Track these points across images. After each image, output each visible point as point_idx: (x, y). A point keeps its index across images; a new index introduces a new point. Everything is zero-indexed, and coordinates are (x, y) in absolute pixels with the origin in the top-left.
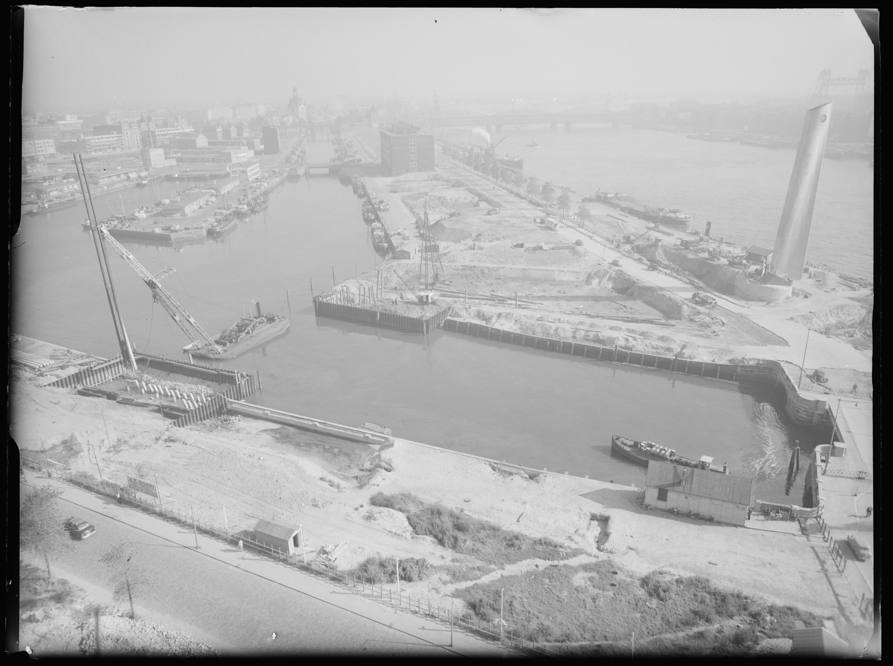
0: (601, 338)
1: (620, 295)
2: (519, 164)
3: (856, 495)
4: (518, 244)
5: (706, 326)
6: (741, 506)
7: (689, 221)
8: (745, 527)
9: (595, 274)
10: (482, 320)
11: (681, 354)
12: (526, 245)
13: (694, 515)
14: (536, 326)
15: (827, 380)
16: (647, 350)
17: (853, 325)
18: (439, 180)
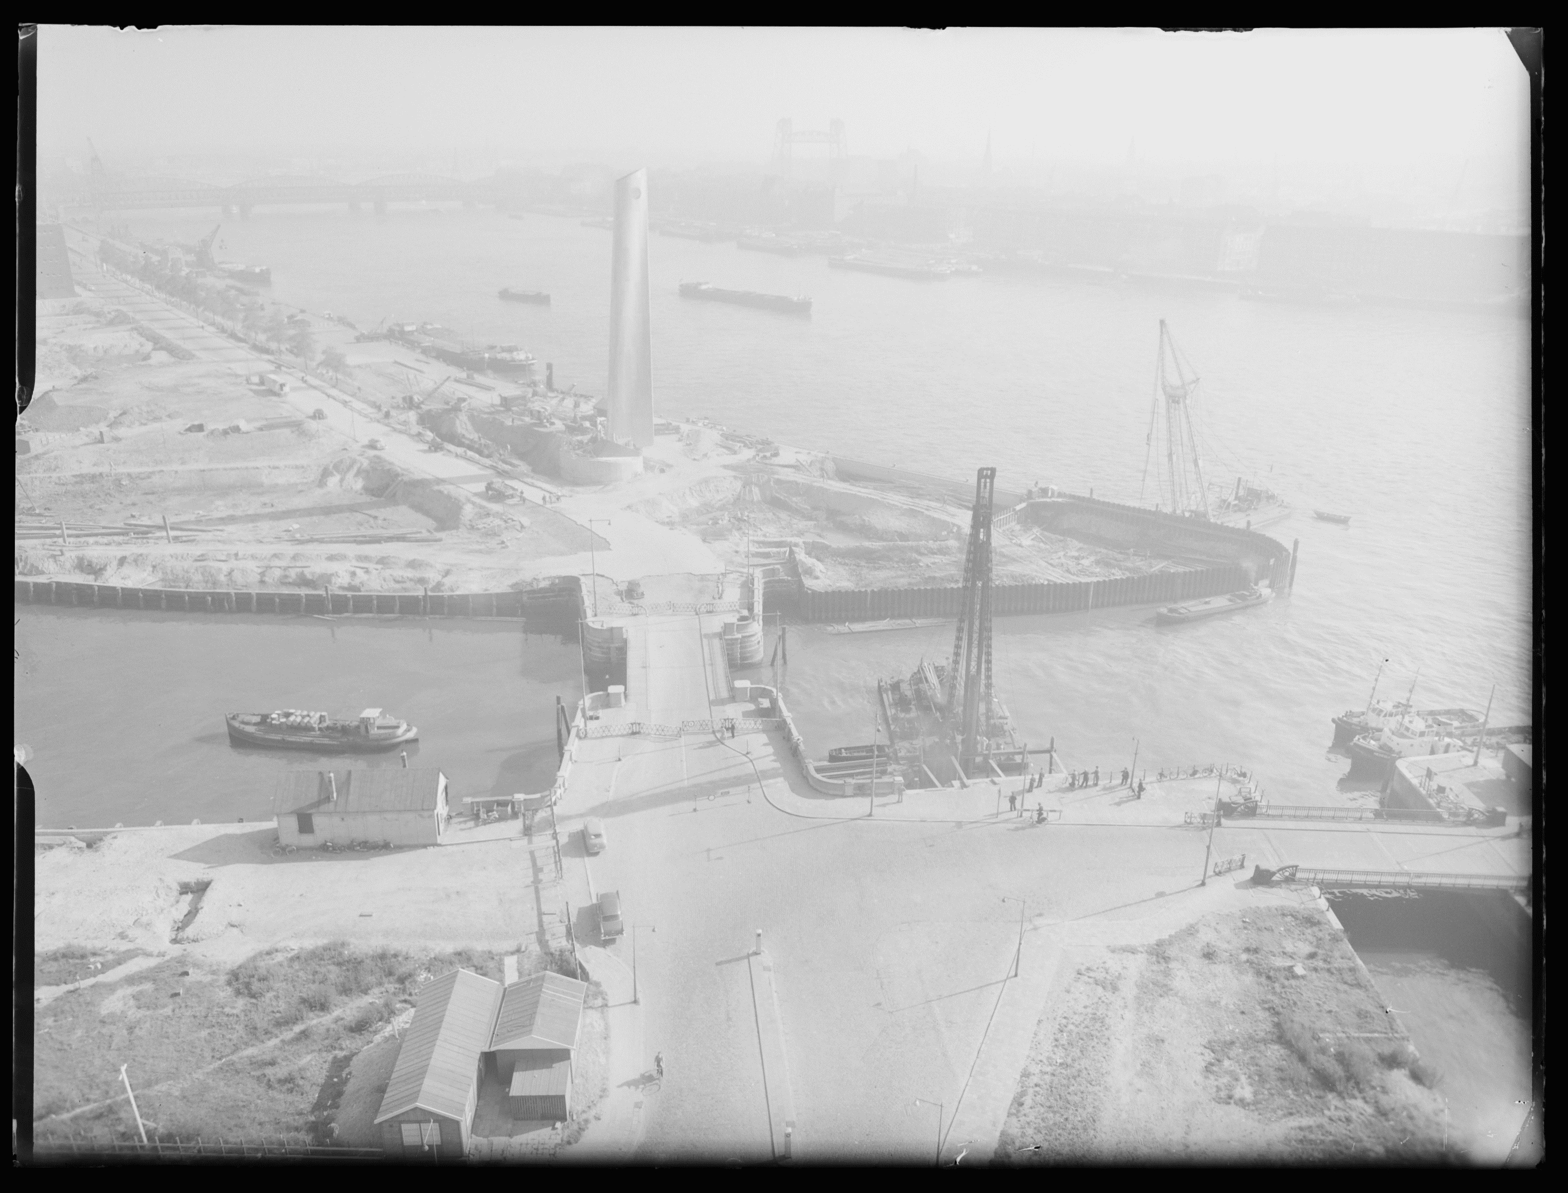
0: (309, 577)
1: (374, 499)
2: (264, 279)
3: (620, 760)
4: (193, 426)
5: (492, 534)
7: (533, 364)
8: (440, 845)
9: (336, 467)
10: (89, 574)
11: (438, 586)
12: (210, 427)
13: (359, 844)
14: (192, 571)
15: (643, 594)
16: (386, 587)
17: (724, 505)
18: (81, 313)
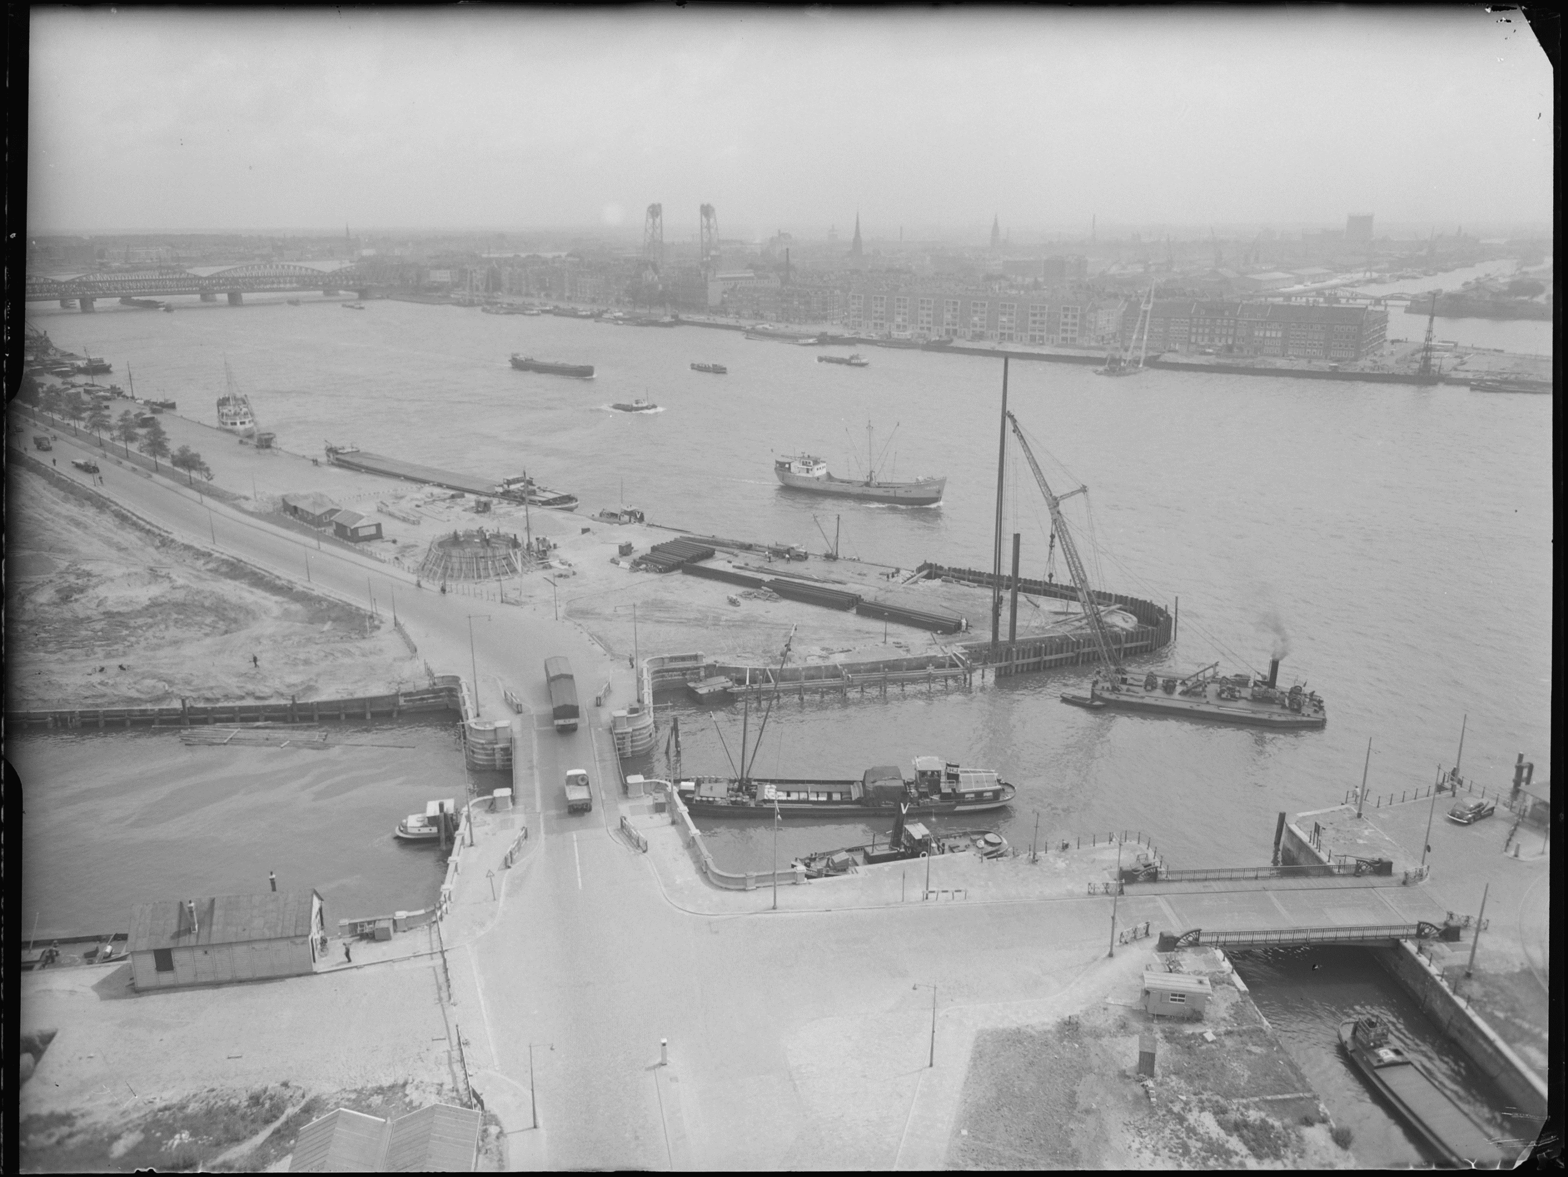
6: (299, 941)
8: (316, 973)
